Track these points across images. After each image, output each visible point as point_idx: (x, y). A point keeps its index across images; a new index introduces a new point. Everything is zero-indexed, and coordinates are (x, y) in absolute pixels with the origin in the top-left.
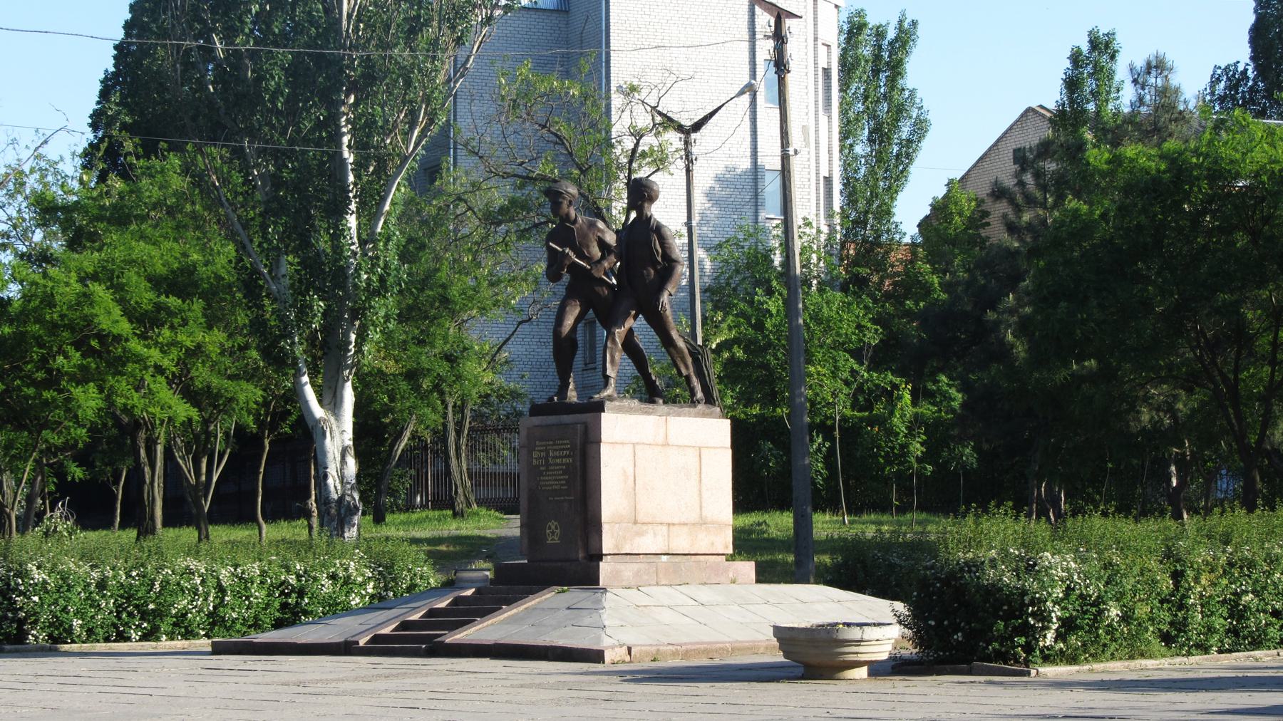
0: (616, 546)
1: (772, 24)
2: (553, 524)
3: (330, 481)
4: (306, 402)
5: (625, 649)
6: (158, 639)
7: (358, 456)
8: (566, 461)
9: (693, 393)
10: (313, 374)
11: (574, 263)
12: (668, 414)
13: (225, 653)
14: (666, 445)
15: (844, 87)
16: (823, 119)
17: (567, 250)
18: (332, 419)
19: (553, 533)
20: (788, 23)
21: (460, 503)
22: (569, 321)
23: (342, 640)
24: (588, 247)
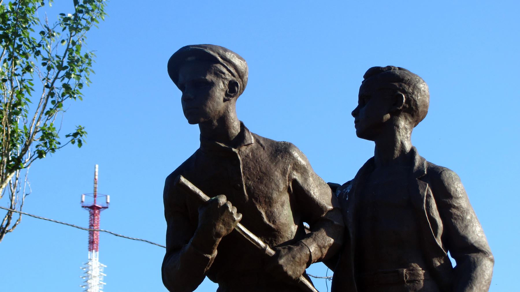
11: (236, 235)
24: (269, 202)
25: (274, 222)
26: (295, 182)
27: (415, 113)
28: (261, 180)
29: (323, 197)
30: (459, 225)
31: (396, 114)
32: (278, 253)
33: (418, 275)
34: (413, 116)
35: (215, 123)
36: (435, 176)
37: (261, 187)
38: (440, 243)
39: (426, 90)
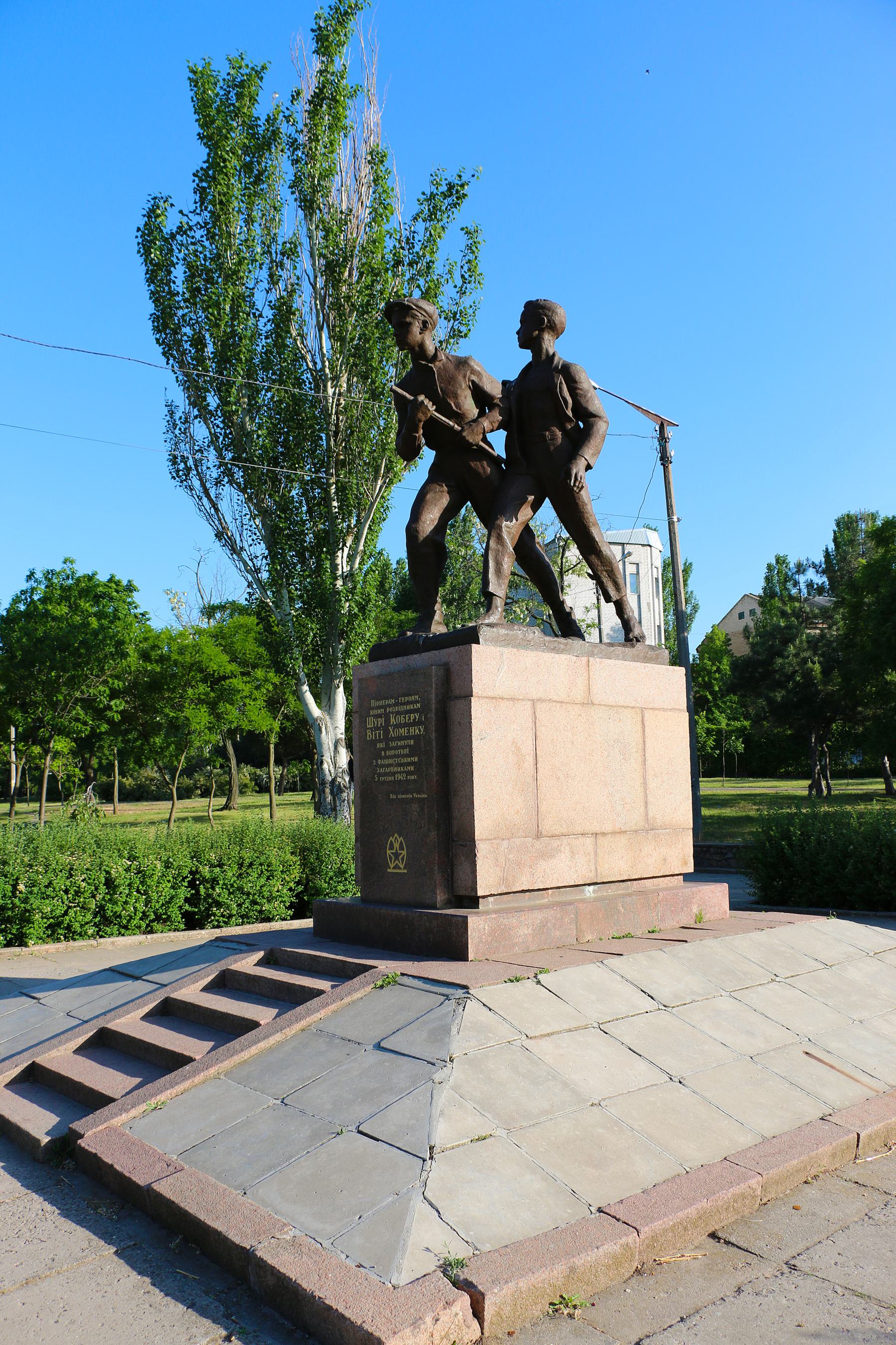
0: (504, 880)
1: (657, 429)
2: (396, 840)
3: (325, 766)
7: (349, 747)
8: (415, 731)
11: (432, 420)
13: (53, 981)
14: (588, 703)
15: (664, 590)
16: (656, 600)
17: (421, 398)
18: (328, 718)
19: (397, 855)
22: (430, 519)
24: (456, 396)
25: (460, 409)
26: (473, 382)
27: (555, 329)
28: (449, 383)
29: (495, 390)
30: (583, 401)
31: (542, 331)
32: (463, 428)
33: (556, 435)
34: (553, 331)
35: (417, 348)
36: (566, 371)
37: (450, 387)
38: (570, 413)
39: (563, 314)
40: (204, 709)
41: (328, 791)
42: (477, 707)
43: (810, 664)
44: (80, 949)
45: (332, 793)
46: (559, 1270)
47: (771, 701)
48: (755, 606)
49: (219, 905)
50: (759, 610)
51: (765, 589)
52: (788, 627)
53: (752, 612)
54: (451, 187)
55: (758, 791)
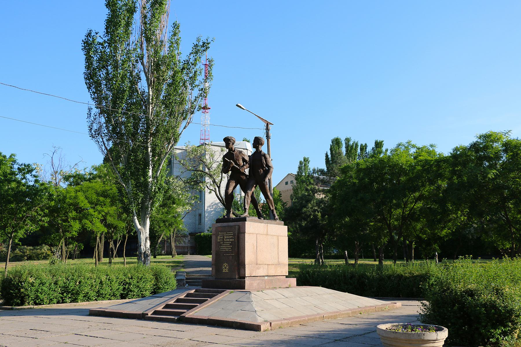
2: (225, 265)
3: (142, 247)
4: (136, 224)
5: (268, 324)
6: (77, 302)
9: (275, 216)
10: (138, 216)
11: (234, 166)
12: (268, 223)
14: (267, 235)
19: (225, 268)
20: (270, 126)
21: (173, 253)
23: (141, 312)
24: (239, 160)
29: (247, 159)
40: (77, 221)
41: (143, 256)
42: (246, 235)
43: (317, 213)
44: (93, 304)
45: (144, 257)
46: (280, 322)
47: (300, 225)
48: (293, 179)
49: (131, 291)
50: (295, 182)
51: (298, 172)
52: (309, 195)
53: (292, 182)
54: (204, 43)
55: (294, 263)
